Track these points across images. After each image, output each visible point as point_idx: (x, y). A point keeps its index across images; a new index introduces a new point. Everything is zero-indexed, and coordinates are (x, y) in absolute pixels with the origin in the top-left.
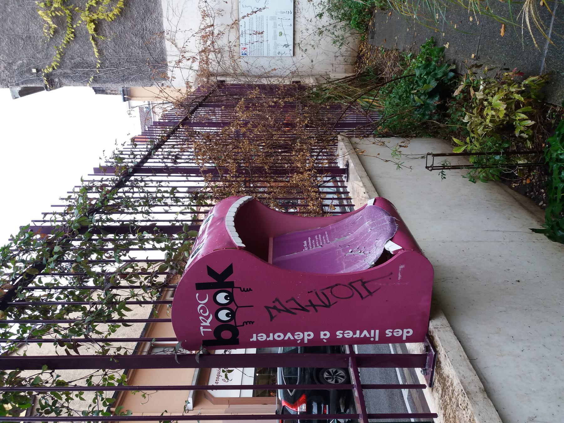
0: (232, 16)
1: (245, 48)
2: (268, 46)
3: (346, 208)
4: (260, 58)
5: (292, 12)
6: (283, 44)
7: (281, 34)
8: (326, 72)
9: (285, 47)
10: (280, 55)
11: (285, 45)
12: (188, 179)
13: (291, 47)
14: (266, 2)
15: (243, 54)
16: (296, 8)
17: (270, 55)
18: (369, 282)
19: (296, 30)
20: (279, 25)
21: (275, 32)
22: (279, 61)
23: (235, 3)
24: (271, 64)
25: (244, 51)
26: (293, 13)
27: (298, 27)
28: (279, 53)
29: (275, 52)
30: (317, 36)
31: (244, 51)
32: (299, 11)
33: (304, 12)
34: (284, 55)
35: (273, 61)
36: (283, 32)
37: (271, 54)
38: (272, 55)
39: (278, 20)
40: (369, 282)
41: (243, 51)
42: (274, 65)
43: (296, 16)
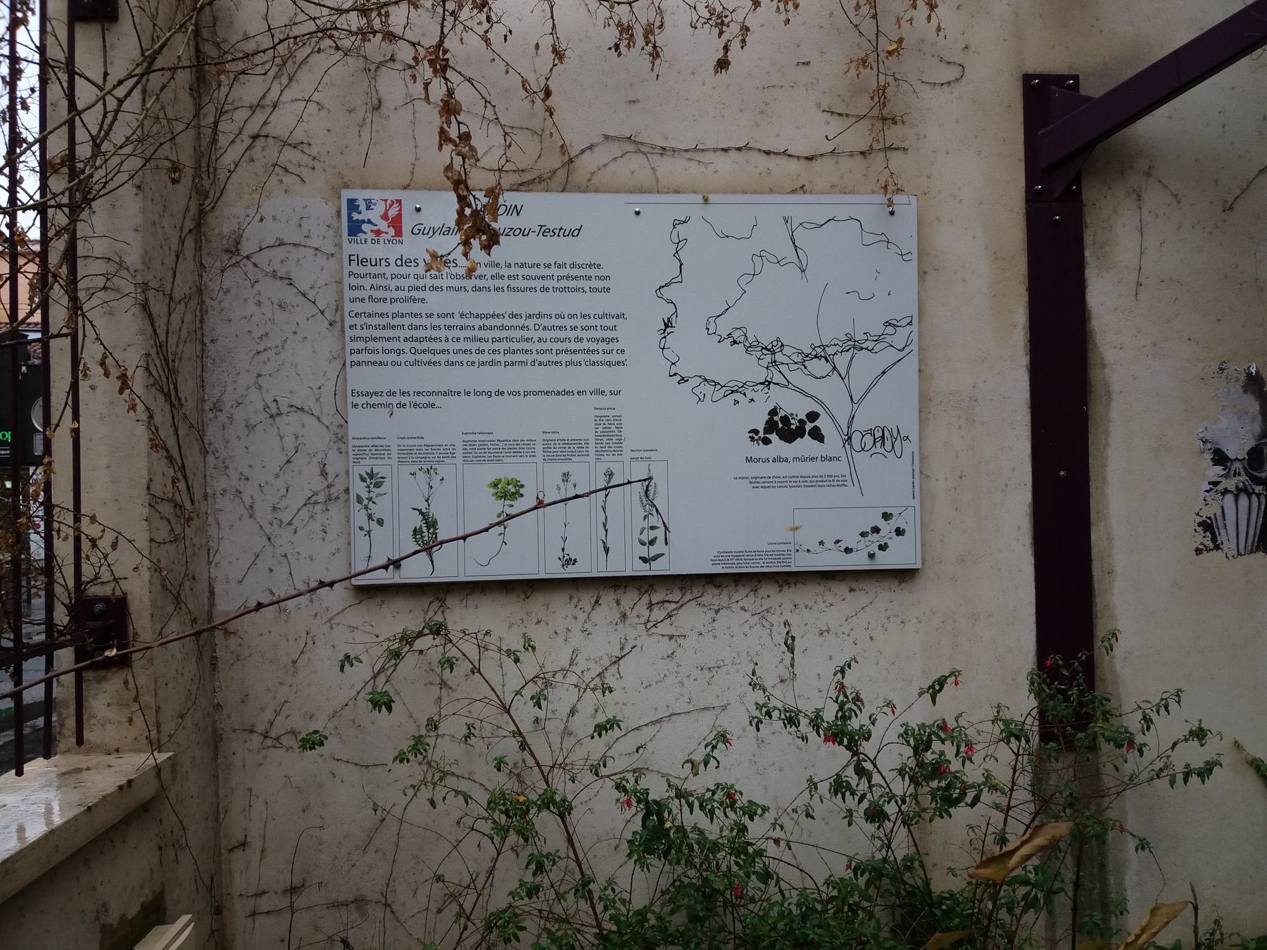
0: (616, 149)
1: (396, 223)
2: (425, 400)
3: (40, 722)
4: (329, 344)
5: (658, 568)
6: (436, 511)
7: (508, 491)
8: (243, 845)
9: (418, 521)
10: (359, 488)
11: (431, 524)
12: (58, 234)
13: (416, 570)
14: (708, 389)
15: (353, 205)
16: (676, 596)
17: (352, 414)
18: (432, 562)
19: (538, 602)
20: (566, 477)
21: (520, 448)
22: (319, 484)
23: (695, 169)
24: (290, 423)
25: (375, 215)
26: (642, 569)
27: (561, 610)
28: (374, 480)
29: (380, 452)
30: (501, 781)
31: (375, 215)
32: (658, 614)
33: (655, 646)
34: (360, 518)
35: (316, 437)
36: (520, 505)
37: (362, 424)
38: (354, 430)
39: (602, 468)
40: (432, 562)
41: (379, 209)
42: (289, 443)
43: (629, 598)
